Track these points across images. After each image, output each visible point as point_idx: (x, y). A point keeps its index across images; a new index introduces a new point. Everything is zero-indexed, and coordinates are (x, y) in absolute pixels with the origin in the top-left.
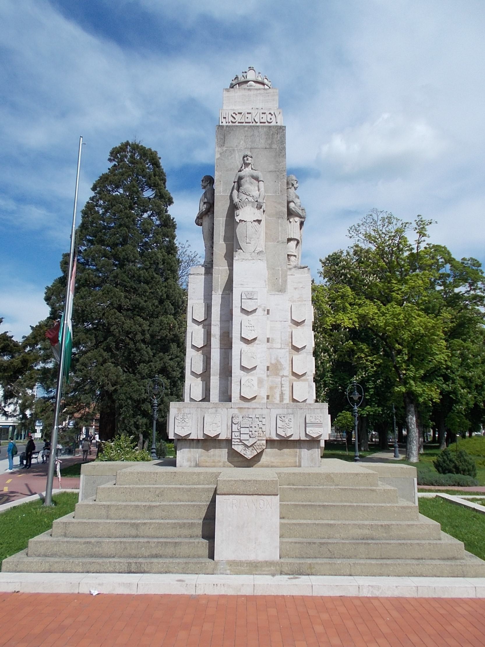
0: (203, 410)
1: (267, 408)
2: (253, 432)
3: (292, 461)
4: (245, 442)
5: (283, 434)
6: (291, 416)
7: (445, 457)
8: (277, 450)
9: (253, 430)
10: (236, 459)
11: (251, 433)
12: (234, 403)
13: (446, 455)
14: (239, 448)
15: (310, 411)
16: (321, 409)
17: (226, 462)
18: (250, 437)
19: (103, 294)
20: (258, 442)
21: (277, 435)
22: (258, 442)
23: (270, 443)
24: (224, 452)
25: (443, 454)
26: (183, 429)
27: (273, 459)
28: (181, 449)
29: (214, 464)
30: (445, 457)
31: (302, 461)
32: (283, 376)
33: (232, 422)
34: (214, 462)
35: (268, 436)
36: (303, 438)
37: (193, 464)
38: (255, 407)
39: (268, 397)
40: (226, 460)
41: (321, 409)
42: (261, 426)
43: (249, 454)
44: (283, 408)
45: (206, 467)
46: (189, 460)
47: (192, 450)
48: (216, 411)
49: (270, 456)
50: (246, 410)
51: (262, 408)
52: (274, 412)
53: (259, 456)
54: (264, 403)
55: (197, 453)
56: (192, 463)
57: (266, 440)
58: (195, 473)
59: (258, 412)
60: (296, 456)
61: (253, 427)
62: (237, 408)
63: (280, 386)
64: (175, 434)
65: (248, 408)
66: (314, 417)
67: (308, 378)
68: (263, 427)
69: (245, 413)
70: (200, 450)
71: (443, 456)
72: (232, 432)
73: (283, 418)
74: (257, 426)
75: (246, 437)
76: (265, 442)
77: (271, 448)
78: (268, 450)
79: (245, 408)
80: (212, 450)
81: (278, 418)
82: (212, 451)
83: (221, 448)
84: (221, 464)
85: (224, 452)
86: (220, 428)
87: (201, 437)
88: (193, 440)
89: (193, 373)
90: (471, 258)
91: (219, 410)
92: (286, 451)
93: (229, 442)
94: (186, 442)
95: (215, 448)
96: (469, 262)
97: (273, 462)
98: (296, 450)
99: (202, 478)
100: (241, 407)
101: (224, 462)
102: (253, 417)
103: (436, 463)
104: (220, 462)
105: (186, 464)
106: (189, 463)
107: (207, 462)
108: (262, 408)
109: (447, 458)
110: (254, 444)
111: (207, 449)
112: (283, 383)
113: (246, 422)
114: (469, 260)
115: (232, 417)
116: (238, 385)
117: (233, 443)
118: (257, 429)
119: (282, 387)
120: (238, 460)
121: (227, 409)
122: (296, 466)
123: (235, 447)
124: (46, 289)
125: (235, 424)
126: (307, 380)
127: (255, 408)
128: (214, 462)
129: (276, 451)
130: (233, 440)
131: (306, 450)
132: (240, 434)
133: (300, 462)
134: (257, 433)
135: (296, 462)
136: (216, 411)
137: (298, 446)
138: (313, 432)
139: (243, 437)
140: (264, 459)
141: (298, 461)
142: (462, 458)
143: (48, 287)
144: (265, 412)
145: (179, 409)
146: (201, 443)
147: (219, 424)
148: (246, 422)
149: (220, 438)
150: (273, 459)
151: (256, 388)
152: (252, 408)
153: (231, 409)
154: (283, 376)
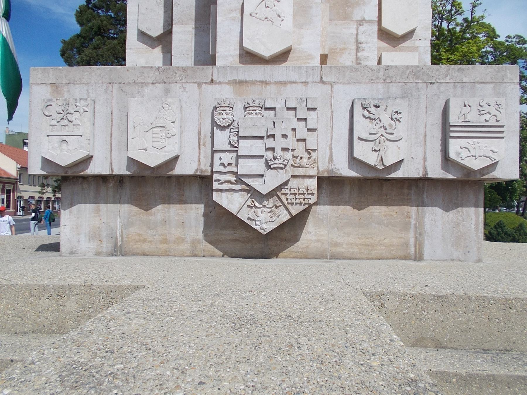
0: (127, 88)
1: (322, 82)
2: (279, 152)
3: (396, 241)
4: (255, 183)
5: (372, 159)
6: (401, 105)
7: (500, 230)
8: (348, 207)
9: (278, 144)
10: (228, 234)
11: (269, 155)
12: (224, 68)
13: (501, 227)
14: (233, 202)
15: (459, 91)
16: (498, 83)
17: (199, 241)
18: (269, 167)
19: (119, 43)
20: (294, 184)
21: (354, 162)
22: (294, 184)
23: (331, 186)
24: (191, 216)
25: (497, 227)
26: (64, 146)
27: (336, 236)
28: (71, 205)
29: (165, 246)
30: (500, 230)
31: (426, 243)
32: (361, 22)
33: (214, 123)
34: (165, 241)
35: (323, 167)
36: (436, 171)
37: (107, 246)
38: (283, 78)
39: (324, 59)
40: (201, 236)
41: (498, 83)
42: (302, 133)
43: (265, 220)
44: (372, 81)
45: (144, 254)
46: (94, 236)
47: (103, 206)
48: (167, 92)
49: (327, 224)
50: (257, 87)
51: (306, 83)
52: (345, 95)
53: (296, 223)
54: (313, 68)
55: (116, 216)
56: (104, 245)
57: (320, 180)
58: (45, 288)
59: (293, 94)
60: (406, 227)
61: (278, 136)
62: (228, 83)
63: (354, 47)
64: (46, 162)
65: (265, 83)
66: (475, 107)
67: (417, 43)
68: (311, 138)
69: (253, 95)
70: (126, 209)
71: (496, 228)
72: (214, 152)
73: (373, 109)
74: (290, 133)
75: (255, 166)
76: (313, 183)
77: (332, 203)
78: (323, 210)
79: (253, 83)
80: (160, 207)
81: (358, 110)
82: (160, 211)
83: (185, 202)
84: (185, 247)
85: (191, 216)
86: (176, 139)
87: (121, 169)
88: (103, 179)
89: (143, 36)
90: (516, 35)
91: (176, 88)
92: (377, 211)
93: (204, 182)
94: (85, 186)
95: (168, 200)
96: (514, 40)
97: (336, 245)
98: (406, 209)
99: (71, 306)
100: (242, 77)
101: (194, 243)
102: (279, 105)
103: (488, 235)
104: (181, 240)
105: (86, 246)
106: (93, 245)
107: (145, 241)
108: (306, 83)
109: (502, 230)
110: (280, 187)
111: (145, 204)
112: (361, 38)
113: (258, 123)
114: (514, 38)
115: (215, 108)
116: (233, 19)
117: (216, 186)
118: (290, 142)
119: (358, 49)
120: (233, 237)
121: (199, 85)
122: (406, 258)
123: (221, 199)
124: (62, 43)
125: (223, 128)
126: (415, 49)
127: (284, 83)
128: (165, 241)
129: (346, 211)
130: (215, 177)
131: (438, 211)
132: (238, 157)
133: (419, 245)
134: (289, 155)
135: (406, 244)
136: (167, 92)
137: (413, 197)
138: (471, 153)
139: (246, 167)
140: (311, 234)
141: (412, 241)
142: (522, 231)
143: (64, 40)
144: (316, 93)
145: (56, 88)
146: (127, 191)
147: (174, 129)
148: (258, 123)
149: (180, 170)
150: (336, 236)
151: (288, 23)
152: (276, 83)
153: (210, 87)
154: (361, 22)
